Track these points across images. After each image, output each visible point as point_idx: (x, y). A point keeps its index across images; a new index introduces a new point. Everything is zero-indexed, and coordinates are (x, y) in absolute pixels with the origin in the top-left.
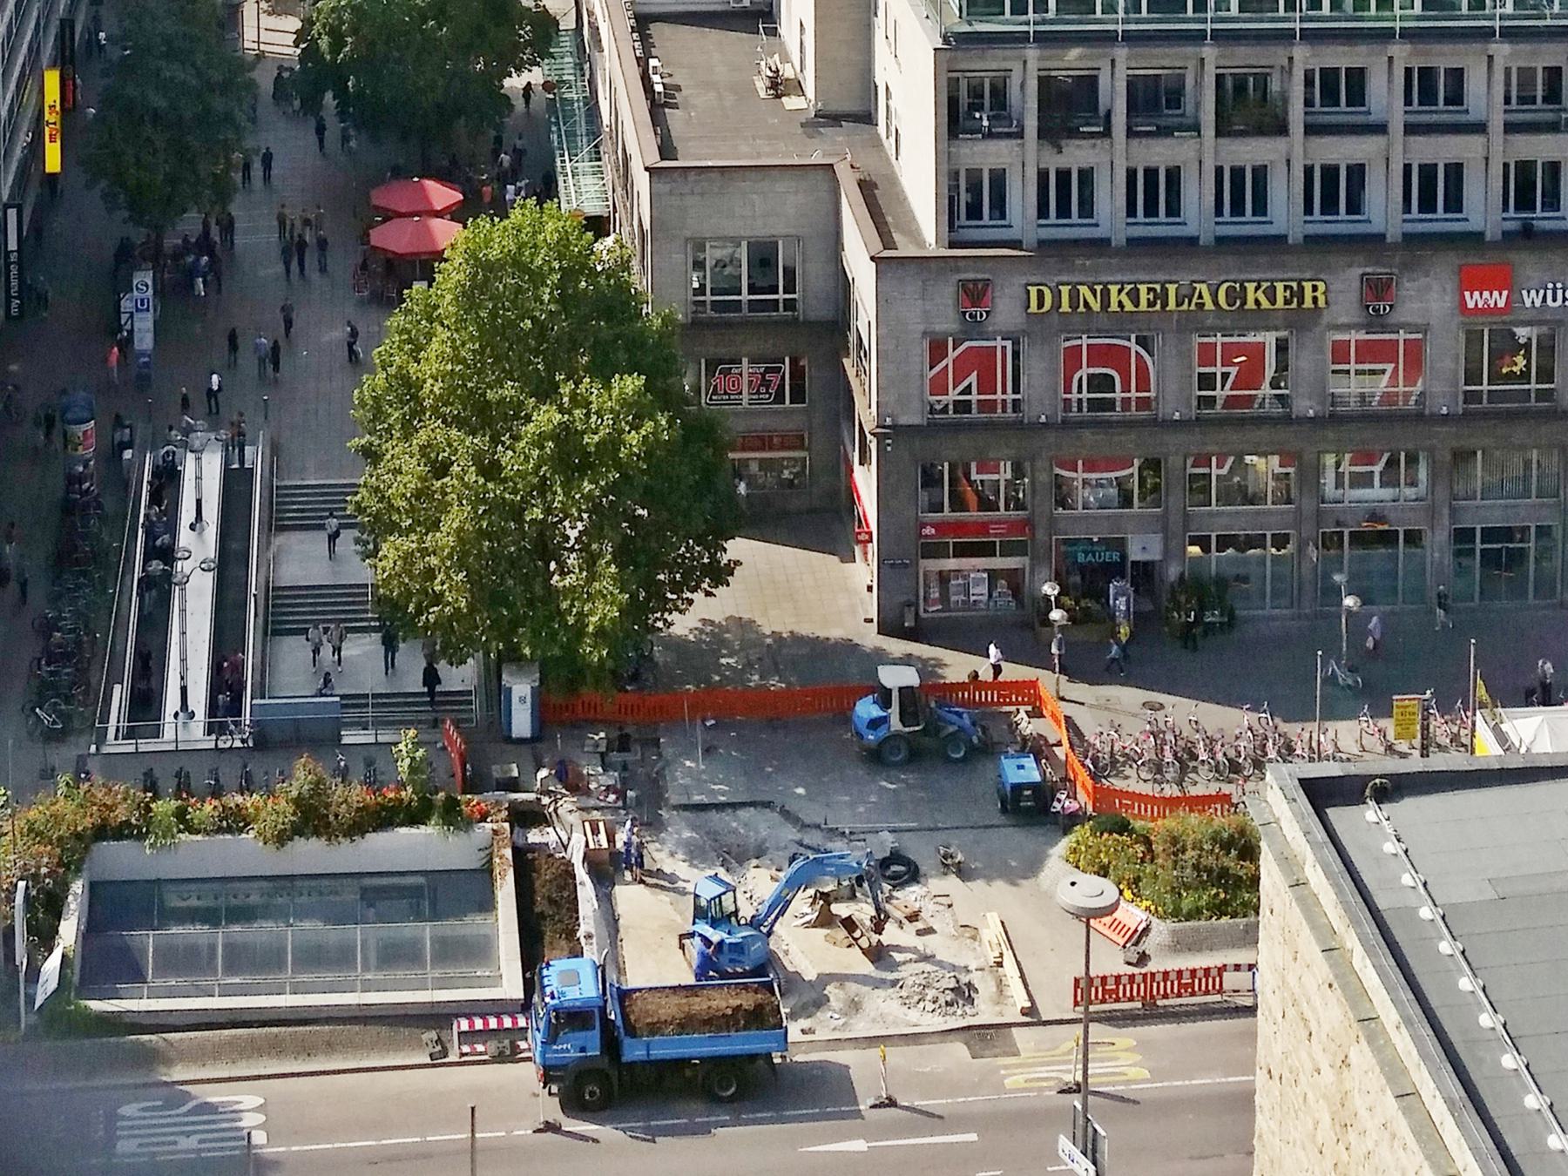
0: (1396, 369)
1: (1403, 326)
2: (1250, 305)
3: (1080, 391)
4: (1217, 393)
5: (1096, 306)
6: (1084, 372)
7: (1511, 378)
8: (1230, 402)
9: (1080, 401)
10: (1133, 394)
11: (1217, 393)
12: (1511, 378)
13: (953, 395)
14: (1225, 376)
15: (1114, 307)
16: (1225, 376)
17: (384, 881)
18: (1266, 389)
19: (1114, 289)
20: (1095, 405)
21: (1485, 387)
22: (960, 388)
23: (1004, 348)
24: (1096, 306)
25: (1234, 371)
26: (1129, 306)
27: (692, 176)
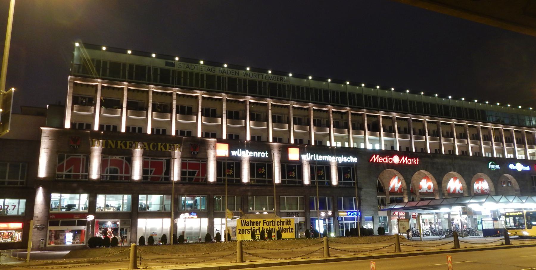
0: (199, 172)
1: (201, 158)
2: (159, 149)
3: (107, 173)
4: (149, 175)
5: (113, 146)
6: (109, 167)
7: (292, 177)
8: (152, 178)
9: (107, 176)
10: (124, 175)
11: (149, 175)
12: (292, 177)
13: (65, 172)
14: (151, 171)
15: (119, 147)
16: (151, 171)
17: (429, 242)
18: (163, 175)
19: (119, 142)
20: (111, 177)
21: (235, 178)
22: (68, 170)
23: (83, 159)
24: (113, 146)
25: (154, 169)
26: (163, 149)
27: (258, 105)
